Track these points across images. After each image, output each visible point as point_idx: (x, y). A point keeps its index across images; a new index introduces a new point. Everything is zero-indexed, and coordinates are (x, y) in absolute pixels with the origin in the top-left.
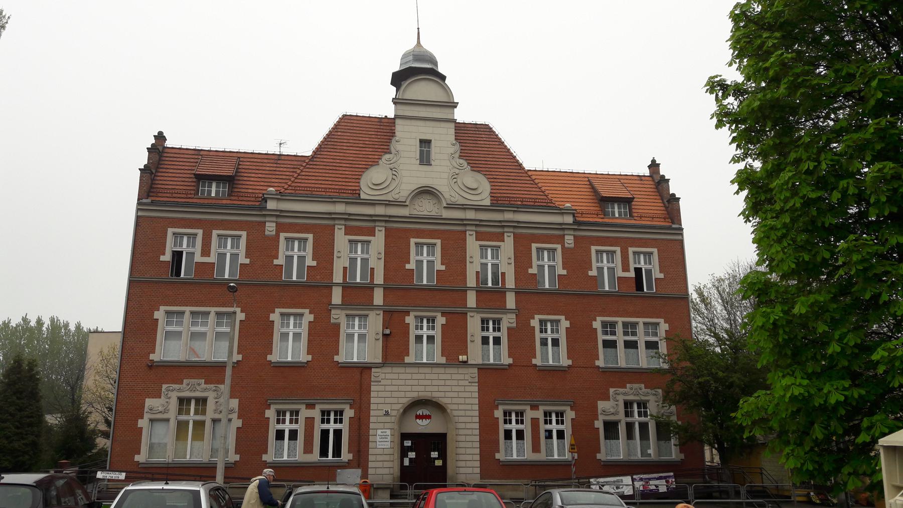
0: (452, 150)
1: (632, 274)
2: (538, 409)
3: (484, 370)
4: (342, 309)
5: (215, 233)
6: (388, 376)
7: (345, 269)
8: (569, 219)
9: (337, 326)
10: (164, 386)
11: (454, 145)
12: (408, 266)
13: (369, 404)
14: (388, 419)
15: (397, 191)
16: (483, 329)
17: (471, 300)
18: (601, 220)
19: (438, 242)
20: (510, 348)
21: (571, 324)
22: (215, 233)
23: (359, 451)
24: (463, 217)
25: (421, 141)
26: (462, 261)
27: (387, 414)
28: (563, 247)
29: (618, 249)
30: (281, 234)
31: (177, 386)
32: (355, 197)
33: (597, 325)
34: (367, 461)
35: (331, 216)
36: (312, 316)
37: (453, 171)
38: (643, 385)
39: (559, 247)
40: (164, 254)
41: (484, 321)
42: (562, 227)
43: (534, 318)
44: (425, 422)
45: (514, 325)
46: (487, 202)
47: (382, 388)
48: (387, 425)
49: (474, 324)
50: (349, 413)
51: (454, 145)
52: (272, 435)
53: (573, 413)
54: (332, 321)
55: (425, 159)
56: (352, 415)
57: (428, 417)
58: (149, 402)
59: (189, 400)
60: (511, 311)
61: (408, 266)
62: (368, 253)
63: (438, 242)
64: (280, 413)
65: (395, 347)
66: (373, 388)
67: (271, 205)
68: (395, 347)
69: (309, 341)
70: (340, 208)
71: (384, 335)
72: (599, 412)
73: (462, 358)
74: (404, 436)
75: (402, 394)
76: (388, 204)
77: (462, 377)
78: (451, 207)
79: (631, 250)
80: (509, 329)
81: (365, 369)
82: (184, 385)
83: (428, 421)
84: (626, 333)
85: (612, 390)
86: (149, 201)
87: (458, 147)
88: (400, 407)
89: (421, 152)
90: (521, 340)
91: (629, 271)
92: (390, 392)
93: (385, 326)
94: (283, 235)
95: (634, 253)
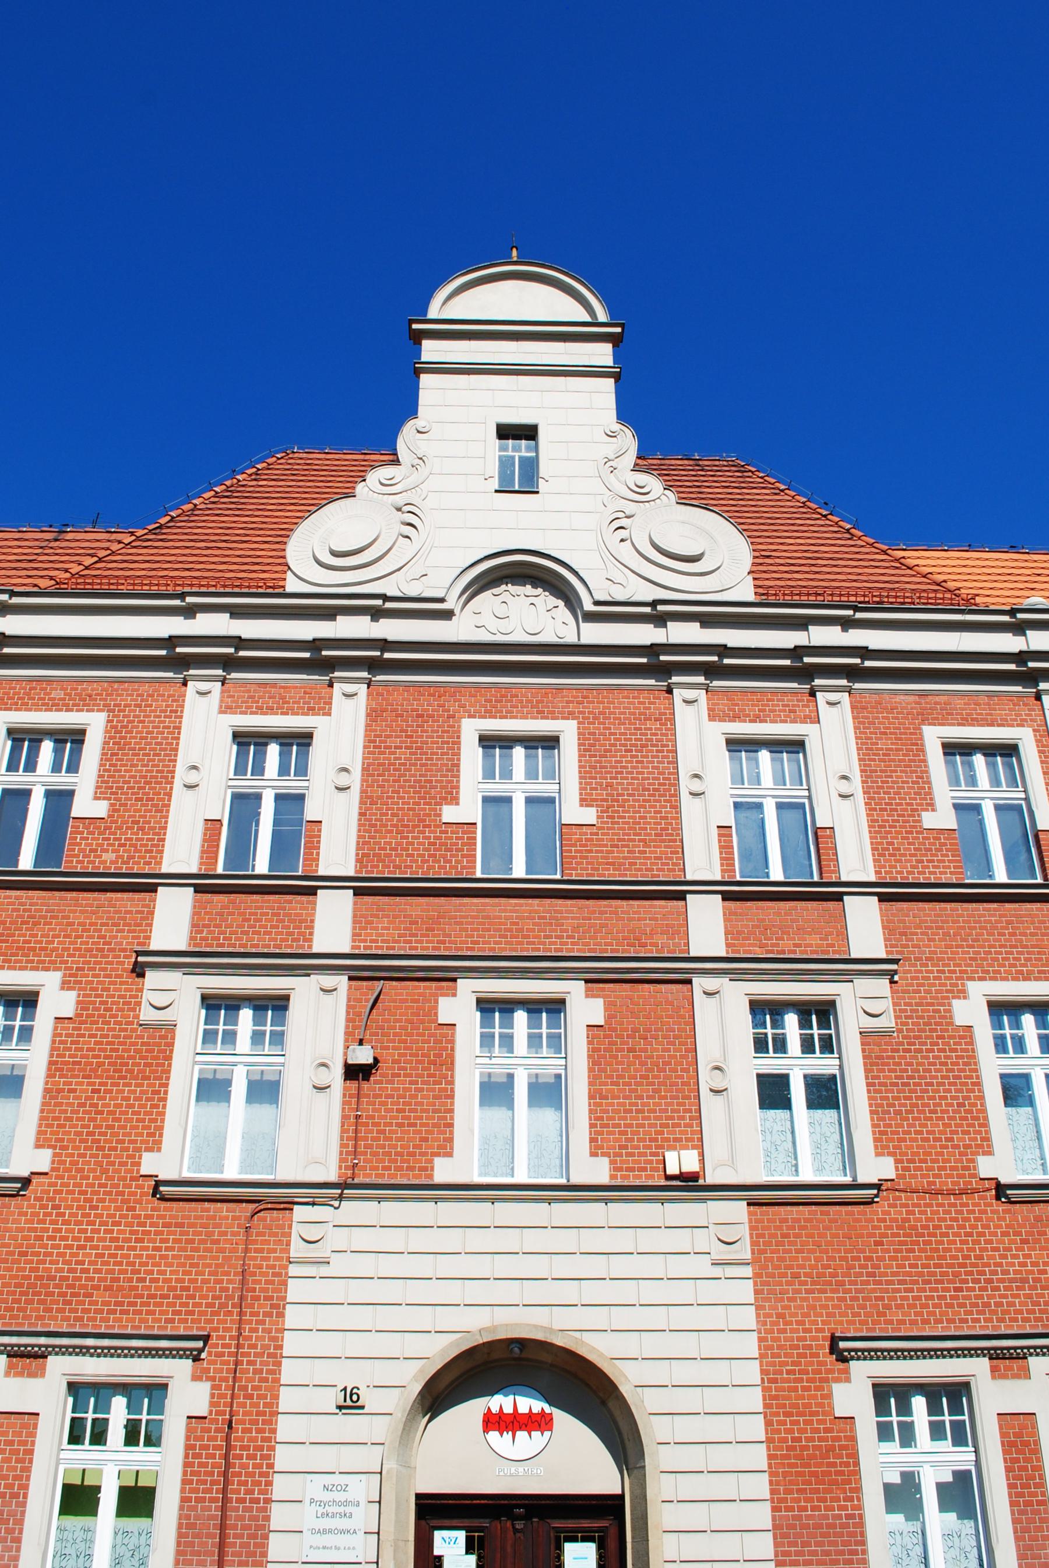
0: (610, 448)
3: (762, 1197)
4: (736, 976)
6: (362, 1239)
7: (212, 826)
9: (163, 1036)
11: (612, 435)
12: (450, 814)
13: (276, 1358)
14: (351, 1425)
16: (760, 1045)
21: (82, 1004)
25: (505, 432)
26: (666, 790)
27: (351, 1403)
35: (176, 658)
36: (71, 996)
43: (963, 994)
44: (526, 1443)
46: (746, 592)
49: (721, 1019)
50: (189, 1395)
51: (612, 435)
54: (147, 1014)
56: (202, 1408)
57: (538, 1423)
60: (868, 967)
61: (450, 814)
62: (302, 770)
65: (392, 1148)
66: (295, 1290)
68: (392, 1148)
71: (354, 1072)
73: (689, 1162)
74: (434, 1510)
75: (423, 1318)
77: (681, 1240)
81: (268, 1202)
87: (628, 442)
88: (412, 1379)
89: (505, 464)
90: (923, 1080)
92: (370, 1303)
93: (355, 1037)
95: (950, 749)
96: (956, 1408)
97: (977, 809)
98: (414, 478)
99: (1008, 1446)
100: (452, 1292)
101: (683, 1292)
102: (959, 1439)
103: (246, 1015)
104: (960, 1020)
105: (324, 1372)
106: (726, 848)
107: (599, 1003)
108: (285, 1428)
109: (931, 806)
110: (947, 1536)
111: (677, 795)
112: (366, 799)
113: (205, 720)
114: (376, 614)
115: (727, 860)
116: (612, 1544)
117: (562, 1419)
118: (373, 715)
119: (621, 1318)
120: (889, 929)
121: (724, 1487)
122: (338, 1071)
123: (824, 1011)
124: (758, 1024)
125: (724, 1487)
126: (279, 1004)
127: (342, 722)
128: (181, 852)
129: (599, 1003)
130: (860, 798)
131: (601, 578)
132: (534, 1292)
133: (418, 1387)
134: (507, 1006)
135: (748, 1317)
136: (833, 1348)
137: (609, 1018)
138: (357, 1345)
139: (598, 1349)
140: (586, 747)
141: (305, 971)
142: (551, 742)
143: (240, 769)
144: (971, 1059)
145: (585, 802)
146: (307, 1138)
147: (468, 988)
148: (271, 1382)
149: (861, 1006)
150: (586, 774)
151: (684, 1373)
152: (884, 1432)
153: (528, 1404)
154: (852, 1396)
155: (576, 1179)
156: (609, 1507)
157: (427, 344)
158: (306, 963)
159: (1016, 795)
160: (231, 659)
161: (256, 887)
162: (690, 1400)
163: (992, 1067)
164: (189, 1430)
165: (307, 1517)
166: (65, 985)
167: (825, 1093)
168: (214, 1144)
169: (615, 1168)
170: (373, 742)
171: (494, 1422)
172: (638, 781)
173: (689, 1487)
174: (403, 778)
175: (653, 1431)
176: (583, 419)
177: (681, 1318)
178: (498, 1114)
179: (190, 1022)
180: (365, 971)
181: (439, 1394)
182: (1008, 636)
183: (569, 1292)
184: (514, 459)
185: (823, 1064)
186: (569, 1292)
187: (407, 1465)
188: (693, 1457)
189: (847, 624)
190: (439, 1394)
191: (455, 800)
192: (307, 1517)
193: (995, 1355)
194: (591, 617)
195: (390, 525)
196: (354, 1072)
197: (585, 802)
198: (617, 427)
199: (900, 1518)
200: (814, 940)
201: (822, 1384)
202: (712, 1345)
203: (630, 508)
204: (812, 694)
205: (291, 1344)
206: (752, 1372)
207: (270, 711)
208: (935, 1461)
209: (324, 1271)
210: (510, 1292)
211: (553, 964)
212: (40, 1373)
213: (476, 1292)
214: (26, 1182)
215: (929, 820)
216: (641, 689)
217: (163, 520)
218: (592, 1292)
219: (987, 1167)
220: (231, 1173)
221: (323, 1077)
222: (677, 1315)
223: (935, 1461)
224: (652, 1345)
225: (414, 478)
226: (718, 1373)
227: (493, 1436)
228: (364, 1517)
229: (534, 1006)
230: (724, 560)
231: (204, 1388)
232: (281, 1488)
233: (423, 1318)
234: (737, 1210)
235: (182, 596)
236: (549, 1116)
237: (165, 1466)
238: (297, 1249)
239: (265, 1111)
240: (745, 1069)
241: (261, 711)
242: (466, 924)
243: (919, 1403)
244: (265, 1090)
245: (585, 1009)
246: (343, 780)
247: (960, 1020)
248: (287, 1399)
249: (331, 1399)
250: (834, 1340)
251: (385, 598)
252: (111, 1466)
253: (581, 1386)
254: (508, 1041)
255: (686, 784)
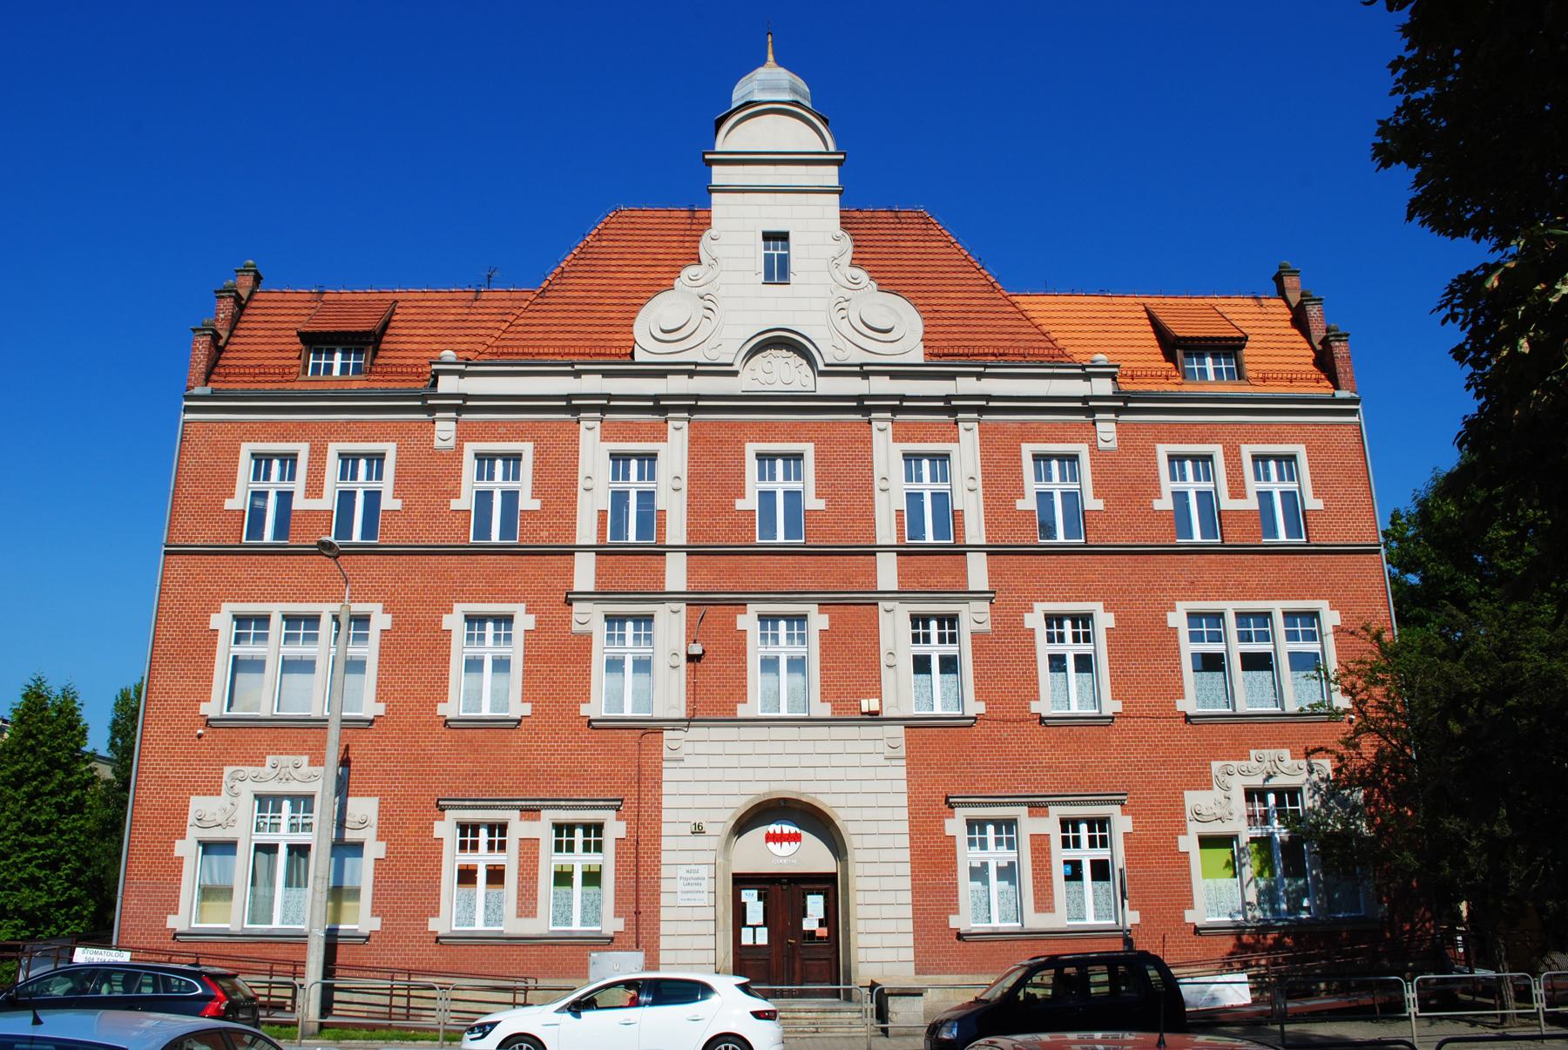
0: (834, 249)
1: (1252, 503)
2: (1046, 815)
3: (913, 725)
5: (334, 449)
6: (700, 748)
8: (1103, 387)
9: (586, 640)
10: (228, 770)
11: (837, 239)
12: (740, 505)
13: (659, 809)
14: (699, 841)
15: (713, 342)
16: (916, 639)
17: (887, 572)
18: (1175, 388)
19: (808, 449)
20: (978, 677)
21: (539, 622)
22: (334, 449)
23: (637, 913)
24: (865, 392)
25: (768, 237)
26: (865, 487)
27: (698, 830)
28: (1094, 450)
29: (1217, 450)
30: (331, 445)
31: (249, 771)
32: (624, 362)
33: (1177, 619)
34: (656, 935)
35: (572, 405)
37: (837, 294)
38: (1286, 753)
39: (1082, 450)
40: (232, 495)
41: (918, 620)
42: (1088, 407)
43: (1031, 610)
44: (788, 848)
45: (987, 627)
46: (917, 356)
47: (687, 774)
48: (700, 857)
49: (894, 625)
50: (615, 829)
51: (837, 239)
52: (449, 876)
53: (1129, 819)
54: (576, 628)
55: (778, 271)
57: (795, 838)
58: (199, 805)
59: (277, 799)
60: (978, 595)
61: (740, 505)
62: (652, 477)
63: (808, 449)
64: (467, 829)
65: (714, 690)
66: (666, 775)
67: (447, 384)
68: (714, 690)
69: (527, 673)
70: (592, 384)
71: (691, 658)
72: (191, 819)
73: (869, 704)
74: (742, 881)
75: (734, 788)
76: (692, 371)
77: (869, 747)
78: (835, 371)
79: (1247, 451)
80: (975, 635)
81: (649, 730)
82: (268, 768)
83: (794, 846)
84: (1245, 637)
85: (1216, 766)
86: (207, 390)
87: (847, 243)
88: (729, 818)
89: (768, 260)
90: (1004, 659)
91: (1244, 496)
92: (705, 781)
94: (470, 449)
96: (1009, 831)
97: (1269, 494)
98: (710, 275)
99: (1034, 850)
100: (749, 774)
101: (870, 773)
102: (1010, 845)
103: (630, 625)
104: (1028, 625)
105: (683, 816)
106: (900, 523)
107: (826, 617)
108: (666, 843)
109: (1022, 496)
110: (1001, 893)
111: (872, 490)
112: (691, 495)
113: (593, 447)
114: (691, 374)
115: (900, 531)
116: (831, 896)
117: (805, 835)
118: (693, 441)
119: (836, 787)
120: (992, 573)
121: (888, 869)
122: (683, 658)
123: (953, 619)
124: (915, 626)
125: (888, 869)
126: (648, 619)
127: (674, 448)
128: (586, 532)
129: (826, 617)
130: (980, 491)
131: (830, 349)
132: (791, 774)
133: (732, 823)
134: (775, 618)
135: (903, 786)
136: (947, 802)
137: (831, 625)
138: (699, 802)
139: (825, 802)
140: (819, 460)
141: (662, 601)
142: (798, 457)
143: (615, 477)
144: (1032, 648)
145: (818, 496)
146: (668, 694)
147: (753, 609)
148: (658, 821)
149: (973, 617)
150: (819, 478)
151: (868, 814)
152: (971, 842)
153: (788, 829)
154: (955, 826)
155: (814, 715)
156: (830, 878)
157: (715, 169)
158: (662, 597)
159: (1074, 486)
160: (605, 405)
161: (630, 558)
162: (872, 827)
163: (1044, 649)
164: (617, 846)
165: (680, 885)
166: (528, 611)
167: (949, 665)
168: (616, 698)
169: (834, 708)
170: (694, 459)
171: (771, 838)
172: (850, 480)
173: (869, 869)
174: (712, 480)
175: (852, 842)
176: (817, 225)
177: (868, 787)
178: (771, 677)
179: (599, 630)
180: (695, 601)
181: (743, 825)
182: (1080, 382)
183: (810, 774)
184: (774, 264)
185: (949, 649)
186: (810, 774)
187: (727, 859)
188: (873, 856)
189: (979, 376)
190: (743, 825)
191: (743, 496)
192: (680, 885)
193: (1031, 805)
194: (822, 374)
195: (695, 310)
196: (691, 658)
197: (818, 496)
198: (840, 233)
199: (979, 884)
200: (948, 579)
201: (940, 820)
202: (883, 800)
203: (848, 294)
204: (956, 423)
205: (666, 802)
206: (904, 814)
207: (631, 439)
208: (997, 856)
209: (681, 764)
210: (779, 774)
211: (801, 596)
212: (538, 818)
213: (760, 774)
214: (519, 721)
215: (1021, 505)
216: (852, 422)
217: (545, 284)
218: (822, 774)
219: (1035, 707)
220: (628, 713)
221: (675, 661)
222: (865, 784)
223: (997, 856)
224: (852, 800)
225: (710, 275)
226: (887, 814)
227: (771, 844)
228: (707, 885)
229: (790, 618)
230: (904, 331)
231: (623, 824)
232: (665, 871)
233: (734, 788)
234: (899, 731)
235: (572, 365)
236: (798, 678)
237: (606, 860)
238: (666, 753)
239: (643, 677)
240: (909, 650)
241: (625, 439)
242: (753, 573)
243: (990, 828)
244: (643, 666)
245: (818, 621)
246: (677, 484)
247: (1028, 625)
248: (665, 829)
249: (688, 829)
250: (947, 798)
251: (696, 364)
252: (579, 861)
253: (810, 818)
254: (776, 637)
255: (878, 484)
